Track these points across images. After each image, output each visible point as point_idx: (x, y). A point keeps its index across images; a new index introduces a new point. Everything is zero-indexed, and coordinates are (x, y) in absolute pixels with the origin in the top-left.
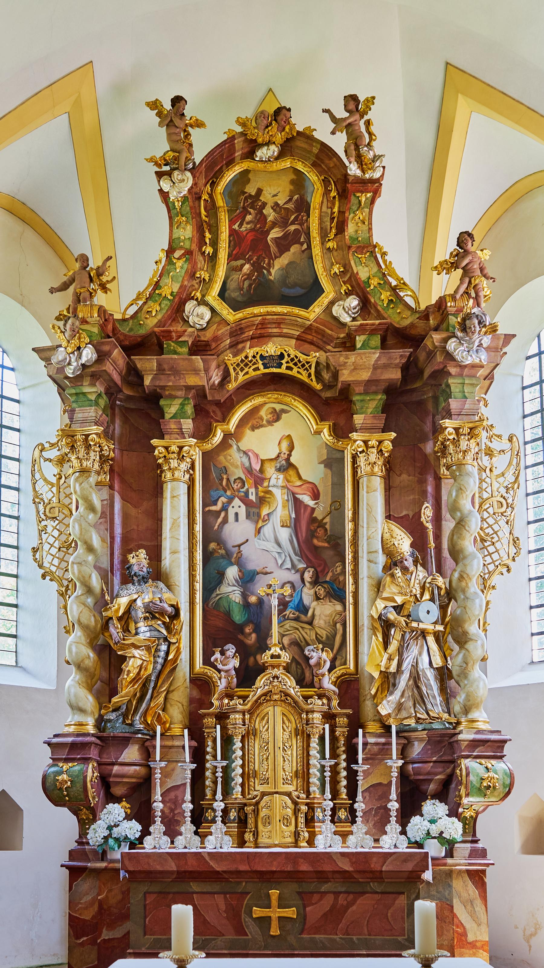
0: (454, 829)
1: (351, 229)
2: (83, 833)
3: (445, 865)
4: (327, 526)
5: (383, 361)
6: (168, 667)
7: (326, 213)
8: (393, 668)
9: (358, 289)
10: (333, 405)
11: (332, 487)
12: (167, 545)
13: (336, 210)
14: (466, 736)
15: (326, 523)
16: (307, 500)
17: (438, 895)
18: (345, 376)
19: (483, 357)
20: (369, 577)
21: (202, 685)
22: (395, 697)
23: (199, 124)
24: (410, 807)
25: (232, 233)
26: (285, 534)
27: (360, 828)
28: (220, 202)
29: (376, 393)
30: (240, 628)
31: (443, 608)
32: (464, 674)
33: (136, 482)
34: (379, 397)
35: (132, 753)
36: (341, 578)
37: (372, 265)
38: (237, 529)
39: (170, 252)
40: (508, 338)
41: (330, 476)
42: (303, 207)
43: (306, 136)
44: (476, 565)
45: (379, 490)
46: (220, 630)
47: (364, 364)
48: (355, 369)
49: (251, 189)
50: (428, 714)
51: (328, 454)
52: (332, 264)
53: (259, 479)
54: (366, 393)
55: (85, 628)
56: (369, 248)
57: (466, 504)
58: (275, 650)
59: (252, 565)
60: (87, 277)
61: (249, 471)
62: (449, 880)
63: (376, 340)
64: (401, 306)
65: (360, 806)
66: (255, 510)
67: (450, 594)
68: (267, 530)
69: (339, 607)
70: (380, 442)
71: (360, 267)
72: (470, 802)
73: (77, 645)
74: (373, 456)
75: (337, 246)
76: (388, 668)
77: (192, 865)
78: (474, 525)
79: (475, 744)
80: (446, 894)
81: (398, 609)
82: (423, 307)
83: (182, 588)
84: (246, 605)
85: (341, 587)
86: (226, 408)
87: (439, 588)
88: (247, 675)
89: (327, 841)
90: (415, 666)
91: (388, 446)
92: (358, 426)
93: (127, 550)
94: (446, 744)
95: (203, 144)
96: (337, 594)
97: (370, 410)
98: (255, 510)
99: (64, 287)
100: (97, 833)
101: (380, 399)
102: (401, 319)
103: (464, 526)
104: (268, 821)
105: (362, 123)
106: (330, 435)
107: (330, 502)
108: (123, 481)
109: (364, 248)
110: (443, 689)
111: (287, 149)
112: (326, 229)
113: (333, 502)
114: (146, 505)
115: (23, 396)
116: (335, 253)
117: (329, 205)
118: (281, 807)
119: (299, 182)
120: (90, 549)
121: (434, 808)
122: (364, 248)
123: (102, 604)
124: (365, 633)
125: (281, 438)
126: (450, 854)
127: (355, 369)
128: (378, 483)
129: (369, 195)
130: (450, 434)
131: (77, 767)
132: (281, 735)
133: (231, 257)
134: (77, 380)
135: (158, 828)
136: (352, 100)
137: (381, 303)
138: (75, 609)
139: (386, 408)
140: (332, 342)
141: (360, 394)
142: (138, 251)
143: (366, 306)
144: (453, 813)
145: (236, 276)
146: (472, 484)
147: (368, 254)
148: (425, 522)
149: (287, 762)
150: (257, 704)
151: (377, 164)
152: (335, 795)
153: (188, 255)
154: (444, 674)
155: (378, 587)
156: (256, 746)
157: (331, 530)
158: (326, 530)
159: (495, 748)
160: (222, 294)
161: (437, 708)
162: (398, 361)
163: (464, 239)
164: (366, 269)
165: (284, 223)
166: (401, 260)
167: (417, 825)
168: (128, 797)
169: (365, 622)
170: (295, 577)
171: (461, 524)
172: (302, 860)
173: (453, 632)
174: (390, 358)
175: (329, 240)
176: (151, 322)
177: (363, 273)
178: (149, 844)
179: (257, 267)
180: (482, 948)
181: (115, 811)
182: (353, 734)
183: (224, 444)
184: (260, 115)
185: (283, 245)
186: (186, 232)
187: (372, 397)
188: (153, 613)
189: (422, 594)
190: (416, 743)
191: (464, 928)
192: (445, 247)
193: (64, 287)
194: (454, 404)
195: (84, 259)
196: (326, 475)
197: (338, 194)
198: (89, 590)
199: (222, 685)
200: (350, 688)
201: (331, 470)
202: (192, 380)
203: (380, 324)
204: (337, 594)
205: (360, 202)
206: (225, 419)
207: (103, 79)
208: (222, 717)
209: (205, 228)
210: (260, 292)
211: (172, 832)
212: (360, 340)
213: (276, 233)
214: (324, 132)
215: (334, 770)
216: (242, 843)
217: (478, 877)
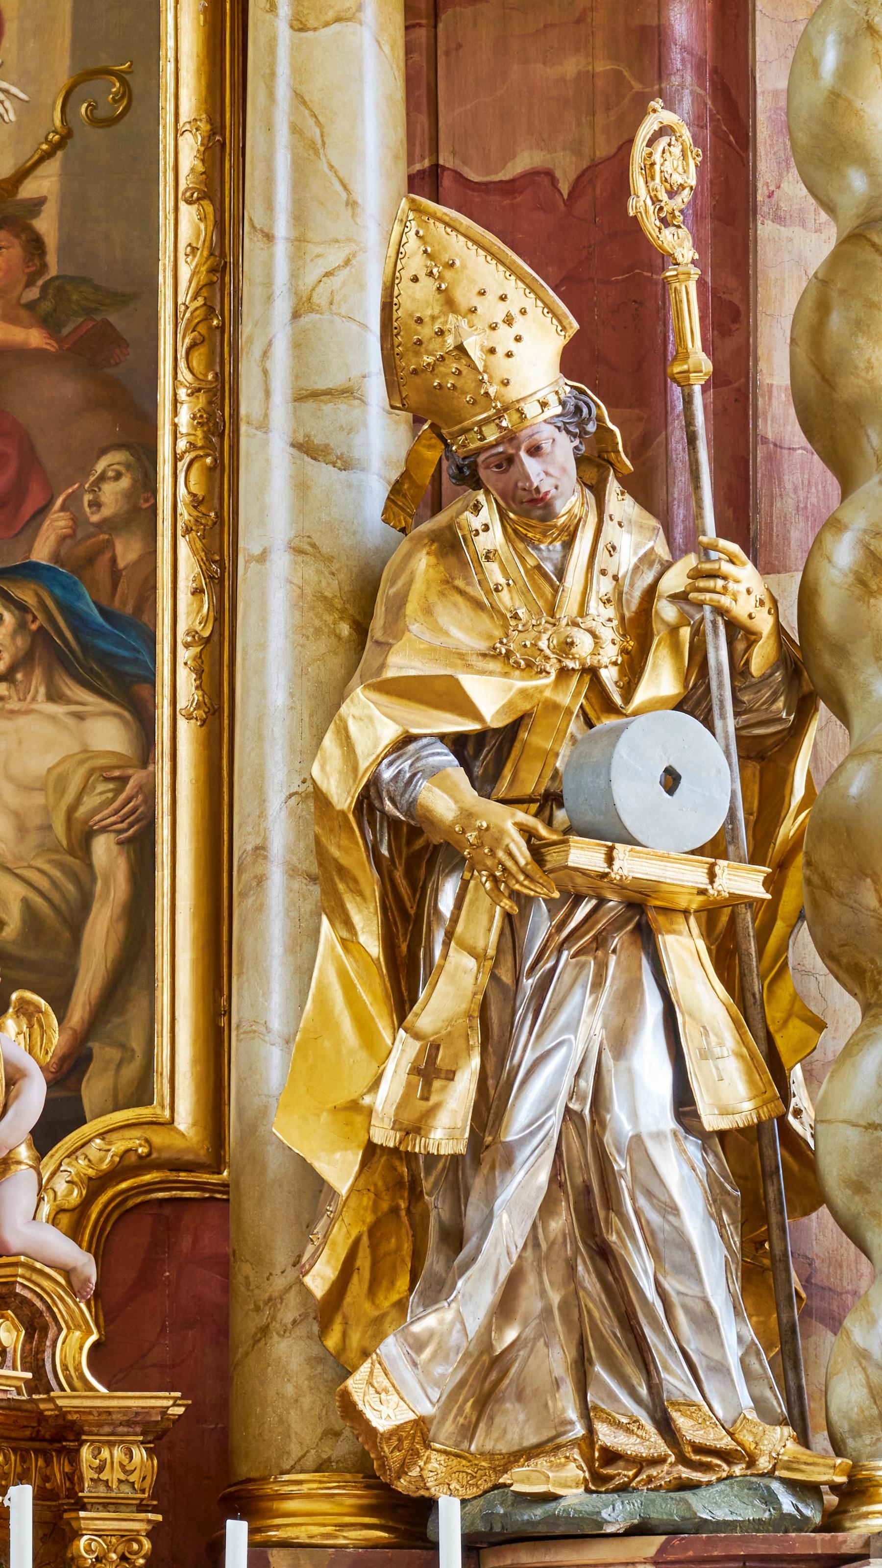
4: (46, 225)
8: (447, 1130)
15: (36, 205)
20: (303, 549)
36: (127, 551)
50: (666, 1427)
69: (109, 734)
76: (415, 1128)
90: (587, 1118)
110: (762, 1270)
113: (84, 77)
124: (273, 904)
148: (651, 224)
155: (359, 613)
157: (66, 246)
158: (35, 245)
169: (272, 828)
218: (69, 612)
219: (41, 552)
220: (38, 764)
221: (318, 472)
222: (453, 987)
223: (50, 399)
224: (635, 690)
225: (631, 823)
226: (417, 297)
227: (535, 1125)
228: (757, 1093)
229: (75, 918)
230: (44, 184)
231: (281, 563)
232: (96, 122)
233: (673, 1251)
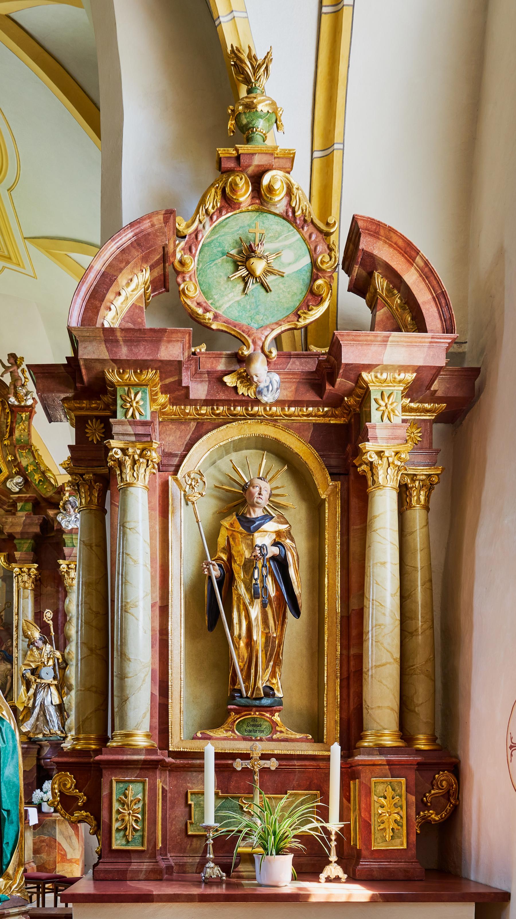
1: (17, 434)
3: (51, 816)
4: (3, 617)
5: (28, 521)
7: (3, 422)
8: (30, 705)
9: (22, 472)
11: (6, 593)
13: (9, 420)
15: (2, 615)
17: (48, 833)
20: (22, 650)
22: (32, 720)
29: (28, 539)
34: (29, 541)
36: (11, 649)
37: (30, 457)
41: (5, 586)
45: (30, 597)
48: (12, 525)
50: (50, 731)
51: (4, 572)
52: (7, 455)
54: (22, 539)
56: (27, 446)
62: (54, 825)
64: (47, 484)
69: (9, 666)
70: (29, 569)
71: (22, 459)
74: (26, 578)
75: (11, 443)
76: (28, 705)
80: (53, 833)
82: (60, 484)
85: (11, 654)
87: (58, 659)
90: (42, 705)
91: (33, 571)
92: (17, 559)
97: (24, 549)
101: (30, 543)
103: (71, 623)
105: (19, 371)
106: (5, 562)
107: (4, 602)
109: (24, 447)
112: (4, 433)
113: (7, 603)
116: (9, 448)
117: (5, 417)
122: (24, 447)
127: (12, 525)
129: (28, 414)
130: (64, 568)
137: (34, 482)
140: (6, 504)
141: (19, 539)
143: (27, 482)
147: (27, 450)
148: (46, 621)
151: (29, 397)
157: (5, 619)
158: (2, 619)
161: (56, 729)
162: (37, 521)
164: (26, 459)
174: (32, 520)
175: (5, 440)
177: (24, 462)
180: (75, 862)
187: (25, 541)
189: (48, 662)
190: (45, 748)
191: (65, 851)
194: (66, 550)
196: (2, 586)
197: (10, 411)
201: (6, 583)
203: (30, 497)
205: (22, 417)
212: (19, 505)
218: (6, 655)
219: (3, 649)
220: (3, 669)
222: (32, 691)
223: (4, 634)
225: (43, 677)
226: (25, 628)
227: (38, 704)
228: (60, 701)
229: (6, 684)
230: (3, 613)
231: (388, 526)
232: (8, 607)
233: (50, 715)
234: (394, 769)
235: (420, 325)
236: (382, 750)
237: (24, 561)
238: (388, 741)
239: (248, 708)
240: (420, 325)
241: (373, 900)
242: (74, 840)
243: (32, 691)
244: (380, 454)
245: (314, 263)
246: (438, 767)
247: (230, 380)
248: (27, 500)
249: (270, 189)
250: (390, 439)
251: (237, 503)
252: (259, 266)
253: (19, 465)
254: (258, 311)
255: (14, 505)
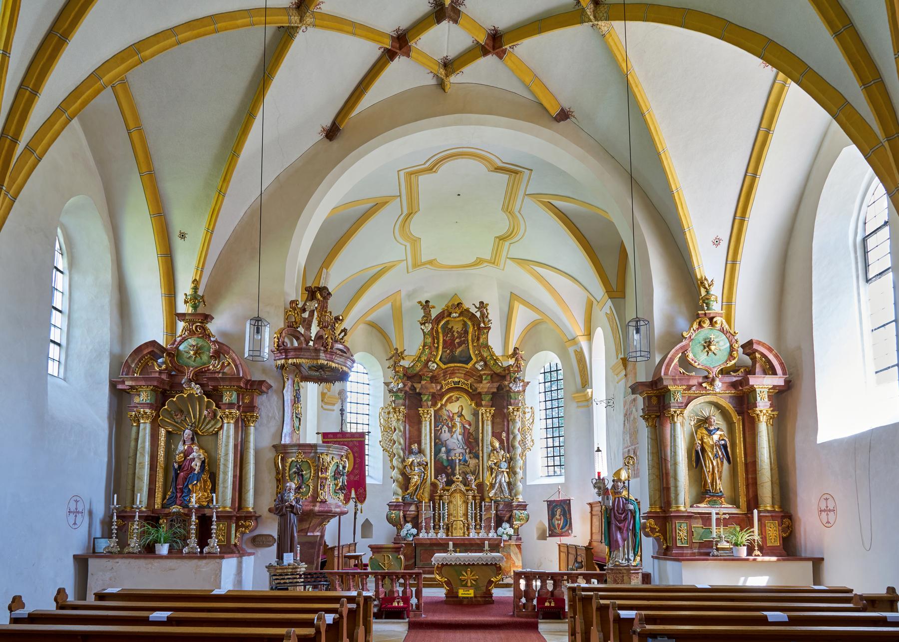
0: (511, 532)
1: (481, 340)
2: (399, 533)
6: (424, 481)
9: (483, 359)
10: (476, 397)
12: (423, 441)
14: (515, 504)
16: (467, 426)
18: (479, 390)
19: (521, 388)
21: (434, 485)
23: (434, 307)
24: (499, 524)
25: (444, 340)
26: (460, 437)
27: (483, 531)
28: (440, 330)
30: (446, 467)
31: (509, 463)
32: (515, 484)
33: (414, 421)
35: (413, 508)
38: (445, 435)
39: (424, 346)
40: (528, 383)
42: (466, 332)
43: (467, 310)
44: (519, 450)
46: (440, 469)
47: (485, 386)
49: (450, 326)
53: (452, 419)
55: (399, 469)
56: (487, 347)
57: (516, 431)
58: (458, 476)
59: (451, 447)
60: (398, 356)
61: (449, 416)
63: (489, 377)
65: (483, 524)
66: (451, 430)
67: (511, 459)
68: (455, 436)
72: (516, 523)
73: (395, 473)
77: (434, 542)
78: (519, 438)
79: (518, 506)
81: (495, 464)
83: (428, 457)
84: (448, 460)
86: (442, 396)
88: (449, 483)
89: (473, 535)
90: (500, 481)
91: (493, 411)
93: (410, 444)
94: (509, 506)
95: (434, 313)
96: (477, 457)
98: (451, 430)
99: (391, 358)
100: (403, 533)
102: (499, 371)
104: (456, 529)
108: (409, 420)
110: (509, 488)
111: (461, 314)
114: (416, 427)
115: (370, 383)
118: (460, 524)
119: (465, 325)
120: (400, 444)
121: (506, 525)
123: (403, 461)
124: (485, 470)
125: (458, 406)
126: (510, 539)
128: (489, 423)
131: (397, 512)
132: (460, 503)
133: (443, 348)
134: (397, 392)
135: (424, 530)
136: (481, 303)
138: (395, 463)
139: (492, 399)
142: (412, 342)
143: (486, 364)
144: (511, 526)
145: (445, 354)
146: (519, 425)
149: (461, 511)
150: (452, 493)
152: (476, 521)
153: (429, 346)
154: (509, 484)
155: (489, 456)
156: (452, 506)
159: (523, 507)
160: (440, 360)
161: (507, 495)
163: (516, 349)
165: (460, 337)
166: (498, 351)
167: (500, 530)
168: (411, 521)
169: (485, 467)
170: (463, 451)
171: (514, 438)
172: (114, 550)
173: (512, 471)
176: (418, 369)
177: (485, 355)
178: (421, 536)
179: (452, 351)
181: (409, 525)
182: (481, 503)
183: (441, 408)
184: (453, 305)
185: (460, 344)
186: (429, 340)
188: (419, 464)
192: (511, 352)
193: (391, 358)
194: (512, 401)
195: (396, 349)
198: (400, 457)
199: (441, 486)
200: (481, 486)
202: (432, 391)
204: (477, 457)
206: (441, 400)
207: (403, 294)
208: (441, 497)
209: (435, 338)
210: (452, 359)
211: (427, 533)
212: (484, 377)
213: (457, 341)
214: (473, 310)
215: (476, 514)
216: (447, 535)
217: (519, 546)
221: (487, 449)
222: (494, 475)
224: (645, 19)
234: (773, 518)
235: (774, 373)
236: (768, 511)
237: (486, 406)
238: (769, 508)
239: (713, 496)
240: (774, 373)
241: (778, 560)
242: (519, 555)
243: (494, 475)
244: (761, 411)
245: (731, 346)
246: (786, 516)
247: (704, 385)
248: (488, 375)
249: (716, 322)
250: (763, 405)
251: (703, 422)
252: (713, 348)
253: (482, 356)
254: (713, 360)
255: (481, 377)
